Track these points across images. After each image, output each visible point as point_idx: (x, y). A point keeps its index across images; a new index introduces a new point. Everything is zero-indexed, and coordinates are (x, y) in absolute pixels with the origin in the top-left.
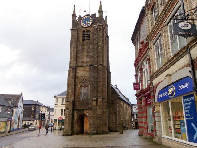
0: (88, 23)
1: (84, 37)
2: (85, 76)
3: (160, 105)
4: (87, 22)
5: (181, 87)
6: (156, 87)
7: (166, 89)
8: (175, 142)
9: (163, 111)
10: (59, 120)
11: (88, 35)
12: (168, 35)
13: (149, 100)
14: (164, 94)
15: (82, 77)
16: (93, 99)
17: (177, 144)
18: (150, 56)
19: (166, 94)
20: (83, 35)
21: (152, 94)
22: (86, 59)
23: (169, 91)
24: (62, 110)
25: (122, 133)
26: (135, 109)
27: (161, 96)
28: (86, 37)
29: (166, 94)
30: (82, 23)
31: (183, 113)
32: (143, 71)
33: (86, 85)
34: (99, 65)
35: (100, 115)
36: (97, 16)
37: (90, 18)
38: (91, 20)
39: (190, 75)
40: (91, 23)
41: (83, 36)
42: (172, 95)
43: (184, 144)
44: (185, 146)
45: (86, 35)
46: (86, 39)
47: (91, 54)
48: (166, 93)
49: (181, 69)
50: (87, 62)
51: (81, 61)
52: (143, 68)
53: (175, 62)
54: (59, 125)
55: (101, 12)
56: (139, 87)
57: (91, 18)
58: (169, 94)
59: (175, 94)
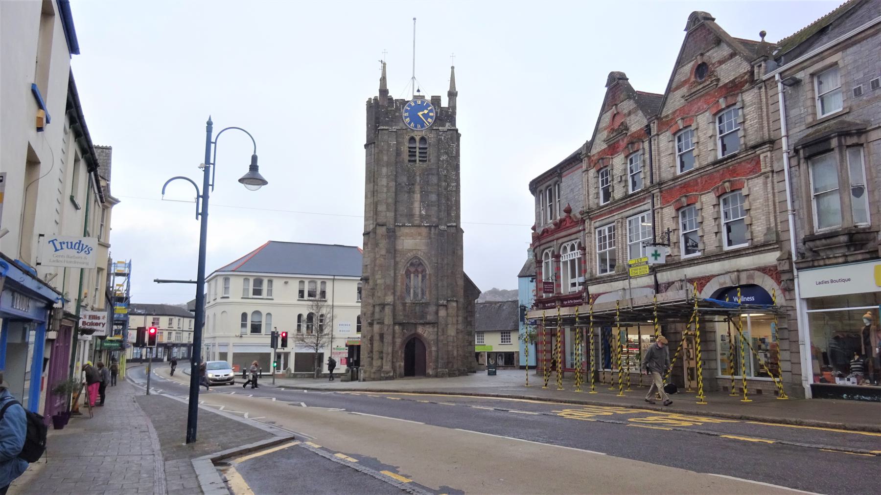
0: (426, 112)
1: (412, 154)
2: (418, 250)
4: (420, 114)
6: (595, 297)
16: (441, 302)
20: (409, 148)
24: (300, 316)
25: (494, 373)
28: (417, 154)
30: (406, 117)
32: (562, 260)
33: (420, 270)
35: (453, 336)
36: (445, 103)
41: (410, 151)
45: (418, 150)
46: (418, 158)
52: (561, 253)
55: (452, 95)
56: (553, 289)
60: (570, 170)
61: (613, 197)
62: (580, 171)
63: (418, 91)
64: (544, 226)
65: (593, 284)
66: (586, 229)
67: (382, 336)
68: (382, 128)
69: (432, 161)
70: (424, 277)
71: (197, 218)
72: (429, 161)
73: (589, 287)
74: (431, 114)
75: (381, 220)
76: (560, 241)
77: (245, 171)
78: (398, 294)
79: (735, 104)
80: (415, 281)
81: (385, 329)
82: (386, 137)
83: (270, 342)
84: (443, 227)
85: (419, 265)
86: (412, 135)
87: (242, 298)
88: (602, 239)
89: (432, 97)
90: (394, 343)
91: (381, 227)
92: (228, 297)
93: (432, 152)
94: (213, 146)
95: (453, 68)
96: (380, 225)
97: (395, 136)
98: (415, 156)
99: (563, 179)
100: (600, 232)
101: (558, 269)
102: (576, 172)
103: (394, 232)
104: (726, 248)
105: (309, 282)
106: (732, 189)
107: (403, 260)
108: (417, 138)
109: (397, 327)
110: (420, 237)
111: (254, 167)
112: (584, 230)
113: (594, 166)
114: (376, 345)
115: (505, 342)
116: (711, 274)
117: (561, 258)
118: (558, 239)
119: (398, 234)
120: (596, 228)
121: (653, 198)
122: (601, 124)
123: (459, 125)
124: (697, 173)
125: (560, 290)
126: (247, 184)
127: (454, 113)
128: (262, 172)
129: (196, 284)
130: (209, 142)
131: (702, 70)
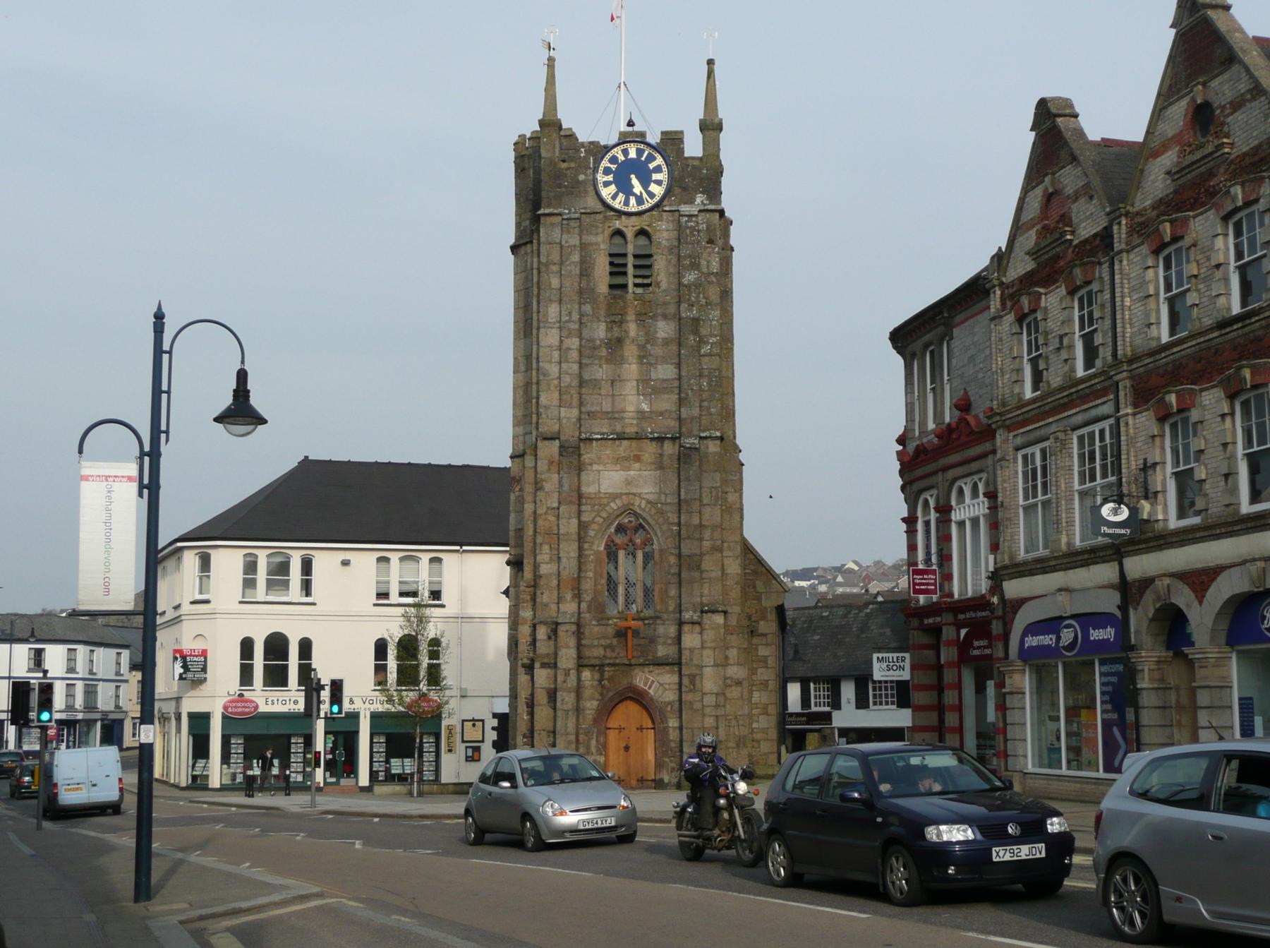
1: (617, 269)
2: (634, 494)
3: (1025, 670)
5: (1096, 635)
7: (1051, 625)
8: (1069, 781)
9: (1035, 690)
10: (224, 717)
11: (644, 262)
12: (1073, 466)
13: (976, 643)
14: (1047, 640)
15: (614, 497)
17: (1073, 785)
18: (1000, 487)
19: (1051, 639)
20: (611, 255)
21: (996, 628)
22: (633, 402)
23: (1062, 635)
24: (381, 648)
26: (884, 665)
27: (1032, 641)
28: (630, 270)
29: (1051, 639)
31: (853, 911)
32: (956, 516)
33: (638, 541)
34: (706, 438)
36: (693, 147)
37: (651, 158)
38: (658, 169)
39: (1118, 613)
40: (658, 190)
41: (611, 264)
42: (1071, 647)
43: (1093, 781)
44: (1095, 784)
45: (630, 261)
47: (665, 372)
48: (1054, 637)
49: (1100, 587)
50: (641, 415)
51: (607, 407)
52: (953, 503)
53: (1086, 564)
54: (226, 758)
55: (711, 127)
57: (659, 161)
58: (1061, 645)
59: (1082, 631)
60: (969, 312)
61: (1048, 382)
62: (986, 315)
63: (631, 123)
64: (920, 437)
65: (1013, 576)
66: (999, 452)
67: (552, 695)
68: (547, 211)
69: (664, 285)
70: (648, 557)
71: (141, 495)
72: (658, 285)
73: (1005, 584)
74: (633, 201)
75: (549, 426)
76: (951, 474)
77: (227, 400)
78: (587, 597)
79: (1257, 201)
80: (629, 568)
81: (560, 679)
82: (556, 234)
83: (137, 781)
84: (692, 440)
85: (636, 531)
86: (617, 224)
87: (241, 602)
88: (1030, 475)
89: (662, 133)
90: (578, 710)
91: (546, 443)
92: (207, 602)
93: (662, 266)
94: (165, 357)
95: (710, 62)
96: (545, 439)
97: (577, 230)
98: (625, 274)
99: (956, 331)
100: (1025, 457)
101: (945, 539)
102: (980, 317)
103: (577, 451)
104: (1246, 508)
105: (402, 559)
106: (1255, 383)
107: (600, 520)
108: (630, 234)
109: (586, 674)
110: (637, 465)
111: (241, 392)
112: (994, 452)
113: (1012, 308)
114: (543, 712)
115: (881, 704)
116: (1219, 562)
117: (953, 512)
118: (945, 469)
119: (586, 457)
120: (1017, 449)
121: (1118, 391)
122: (1024, 213)
123: (728, 202)
124: (1194, 343)
125: (951, 586)
126: (229, 423)
127: (718, 172)
128: (257, 401)
129: (142, 617)
130: (158, 351)
131: (1203, 117)
